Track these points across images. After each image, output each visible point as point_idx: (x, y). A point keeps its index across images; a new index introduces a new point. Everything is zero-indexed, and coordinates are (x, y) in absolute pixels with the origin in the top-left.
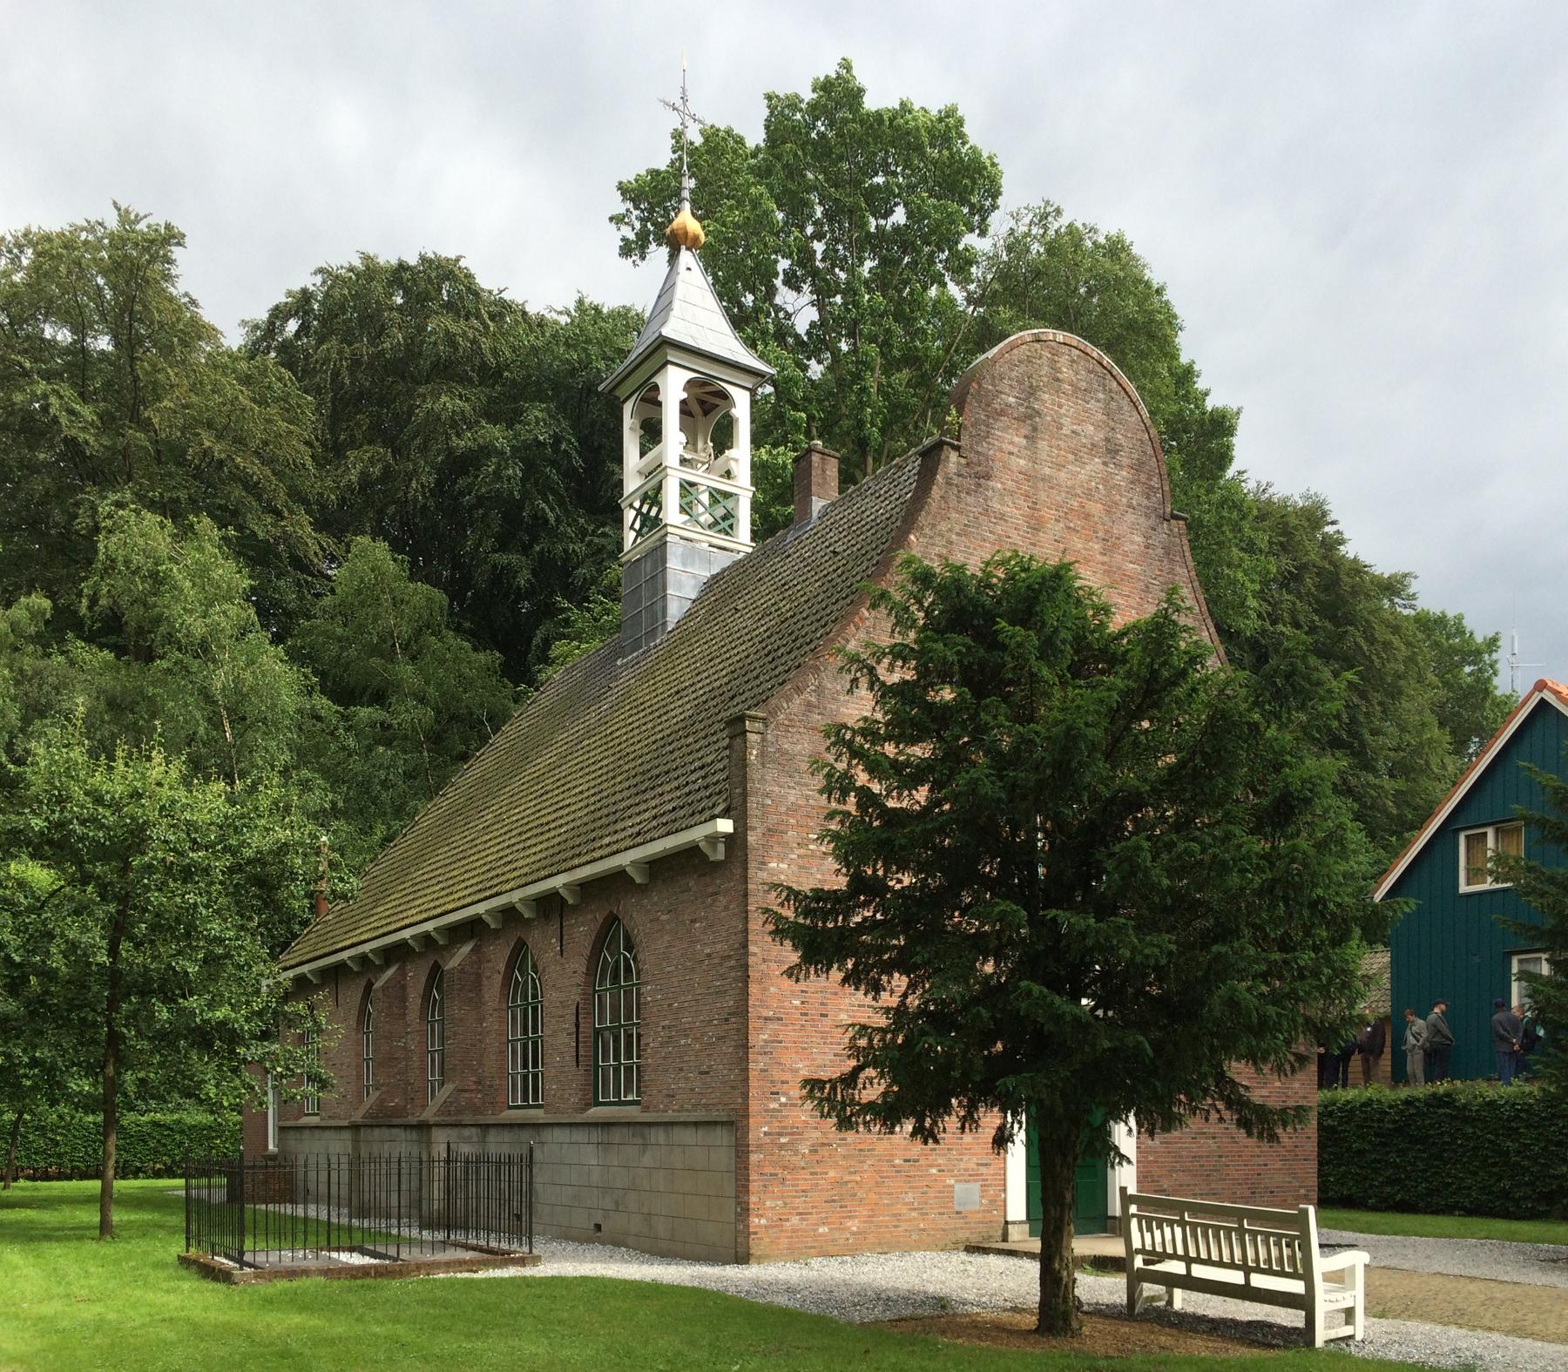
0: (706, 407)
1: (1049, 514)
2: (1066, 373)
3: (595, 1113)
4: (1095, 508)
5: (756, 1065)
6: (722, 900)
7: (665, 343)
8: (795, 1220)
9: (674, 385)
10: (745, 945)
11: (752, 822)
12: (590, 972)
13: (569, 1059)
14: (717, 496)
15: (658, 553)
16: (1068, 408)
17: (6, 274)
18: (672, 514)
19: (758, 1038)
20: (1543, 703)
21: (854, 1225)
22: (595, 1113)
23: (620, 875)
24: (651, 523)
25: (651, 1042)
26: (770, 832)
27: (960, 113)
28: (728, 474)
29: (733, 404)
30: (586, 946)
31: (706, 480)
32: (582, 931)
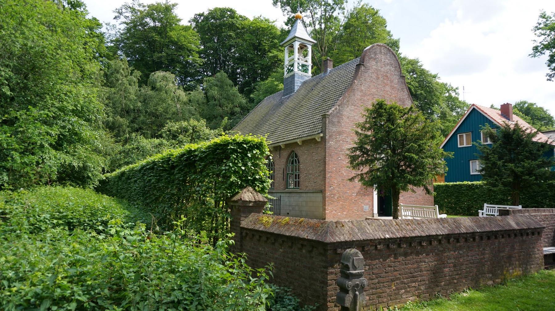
0: (303, 47)
1: (380, 76)
2: (383, 51)
4: (388, 75)
5: (327, 181)
6: (320, 149)
7: (295, 37)
8: (334, 212)
9: (297, 45)
10: (325, 158)
11: (327, 134)
13: (281, 179)
14: (303, 66)
15: (293, 76)
16: (383, 57)
18: (296, 69)
19: (328, 175)
21: (345, 213)
24: (290, 71)
25: (302, 176)
26: (330, 136)
28: (306, 61)
29: (308, 48)
30: (286, 157)
31: (301, 62)
32: (285, 154)
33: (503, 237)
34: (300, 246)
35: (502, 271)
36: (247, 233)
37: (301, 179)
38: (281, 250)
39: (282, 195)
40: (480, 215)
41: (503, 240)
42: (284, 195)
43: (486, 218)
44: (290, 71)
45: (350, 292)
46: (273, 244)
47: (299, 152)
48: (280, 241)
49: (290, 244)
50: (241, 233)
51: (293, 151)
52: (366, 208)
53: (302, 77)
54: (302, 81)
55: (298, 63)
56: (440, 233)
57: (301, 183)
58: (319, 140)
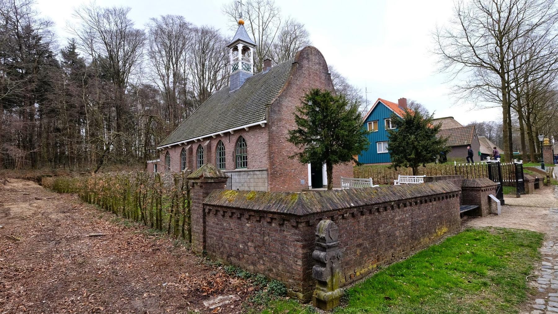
1: (311, 73)
3: (237, 170)
12: (236, 146)
15: (238, 73)
16: (313, 57)
17: (1, 33)
20: (379, 102)
21: (286, 187)
22: (237, 170)
23: (244, 129)
24: (235, 69)
25: (249, 157)
26: (272, 123)
27: (141, 21)
32: (234, 139)
33: (435, 201)
34: (269, 220)
35: (435, 230)
36: (210, 210)
37: (249, 160)
38: (247, 225)
39: (233, 174)
40: (395, 184)
41: (435, 203)
42: (235, 174)
43: (400, 186)
44: (235, 69)
45: (327, 265)
46: (239, 218)
47: (246, 136)
48: (247, 216)
49: (258, 219)
50: (204, 210)
51: (241, 136)
52: (303, 182)
53: (244, 74)
54: (246, 78)
55: (242, 63)
56: (392, 199)
57: (248, 163)
58: (263, 126)
